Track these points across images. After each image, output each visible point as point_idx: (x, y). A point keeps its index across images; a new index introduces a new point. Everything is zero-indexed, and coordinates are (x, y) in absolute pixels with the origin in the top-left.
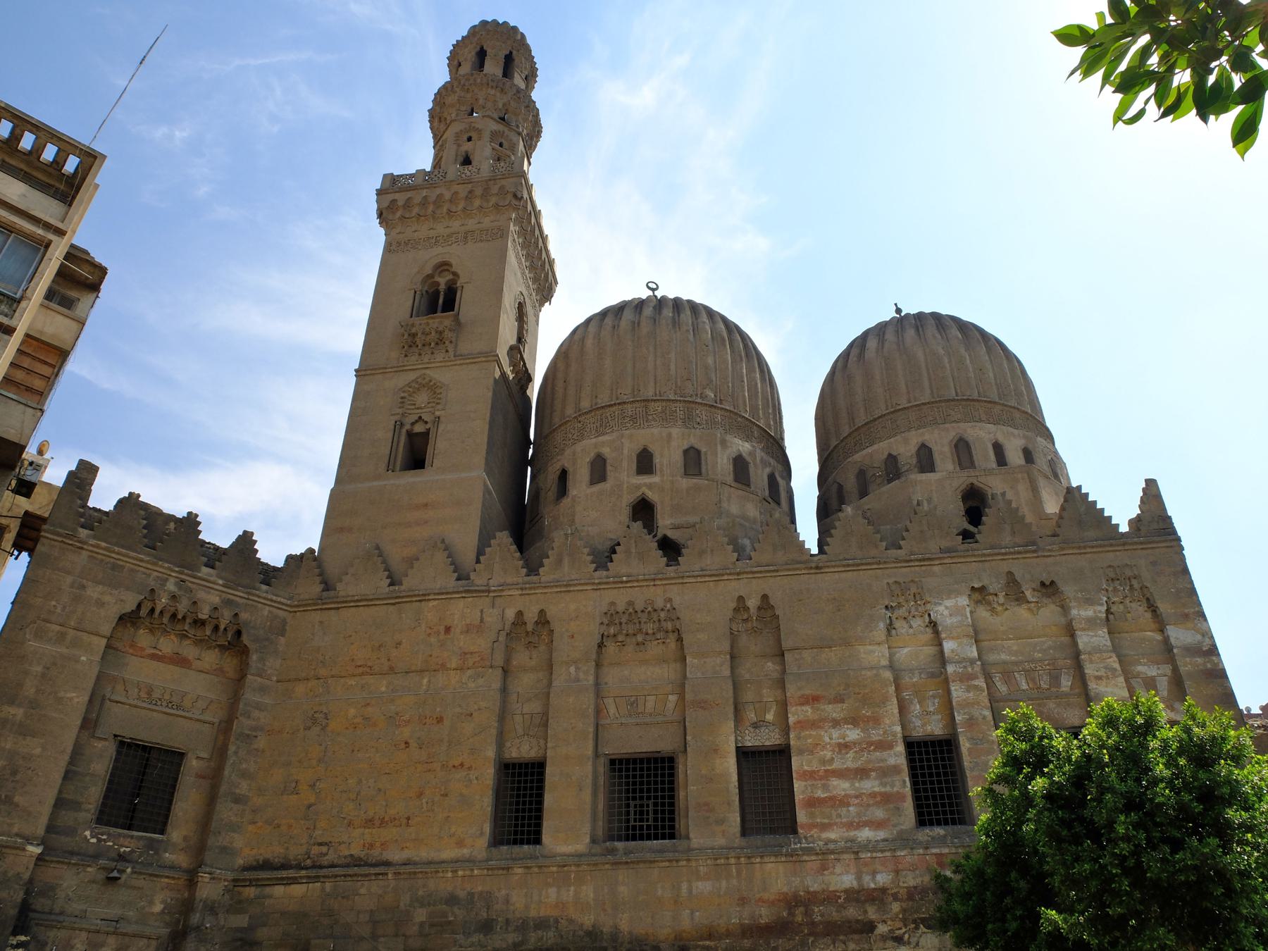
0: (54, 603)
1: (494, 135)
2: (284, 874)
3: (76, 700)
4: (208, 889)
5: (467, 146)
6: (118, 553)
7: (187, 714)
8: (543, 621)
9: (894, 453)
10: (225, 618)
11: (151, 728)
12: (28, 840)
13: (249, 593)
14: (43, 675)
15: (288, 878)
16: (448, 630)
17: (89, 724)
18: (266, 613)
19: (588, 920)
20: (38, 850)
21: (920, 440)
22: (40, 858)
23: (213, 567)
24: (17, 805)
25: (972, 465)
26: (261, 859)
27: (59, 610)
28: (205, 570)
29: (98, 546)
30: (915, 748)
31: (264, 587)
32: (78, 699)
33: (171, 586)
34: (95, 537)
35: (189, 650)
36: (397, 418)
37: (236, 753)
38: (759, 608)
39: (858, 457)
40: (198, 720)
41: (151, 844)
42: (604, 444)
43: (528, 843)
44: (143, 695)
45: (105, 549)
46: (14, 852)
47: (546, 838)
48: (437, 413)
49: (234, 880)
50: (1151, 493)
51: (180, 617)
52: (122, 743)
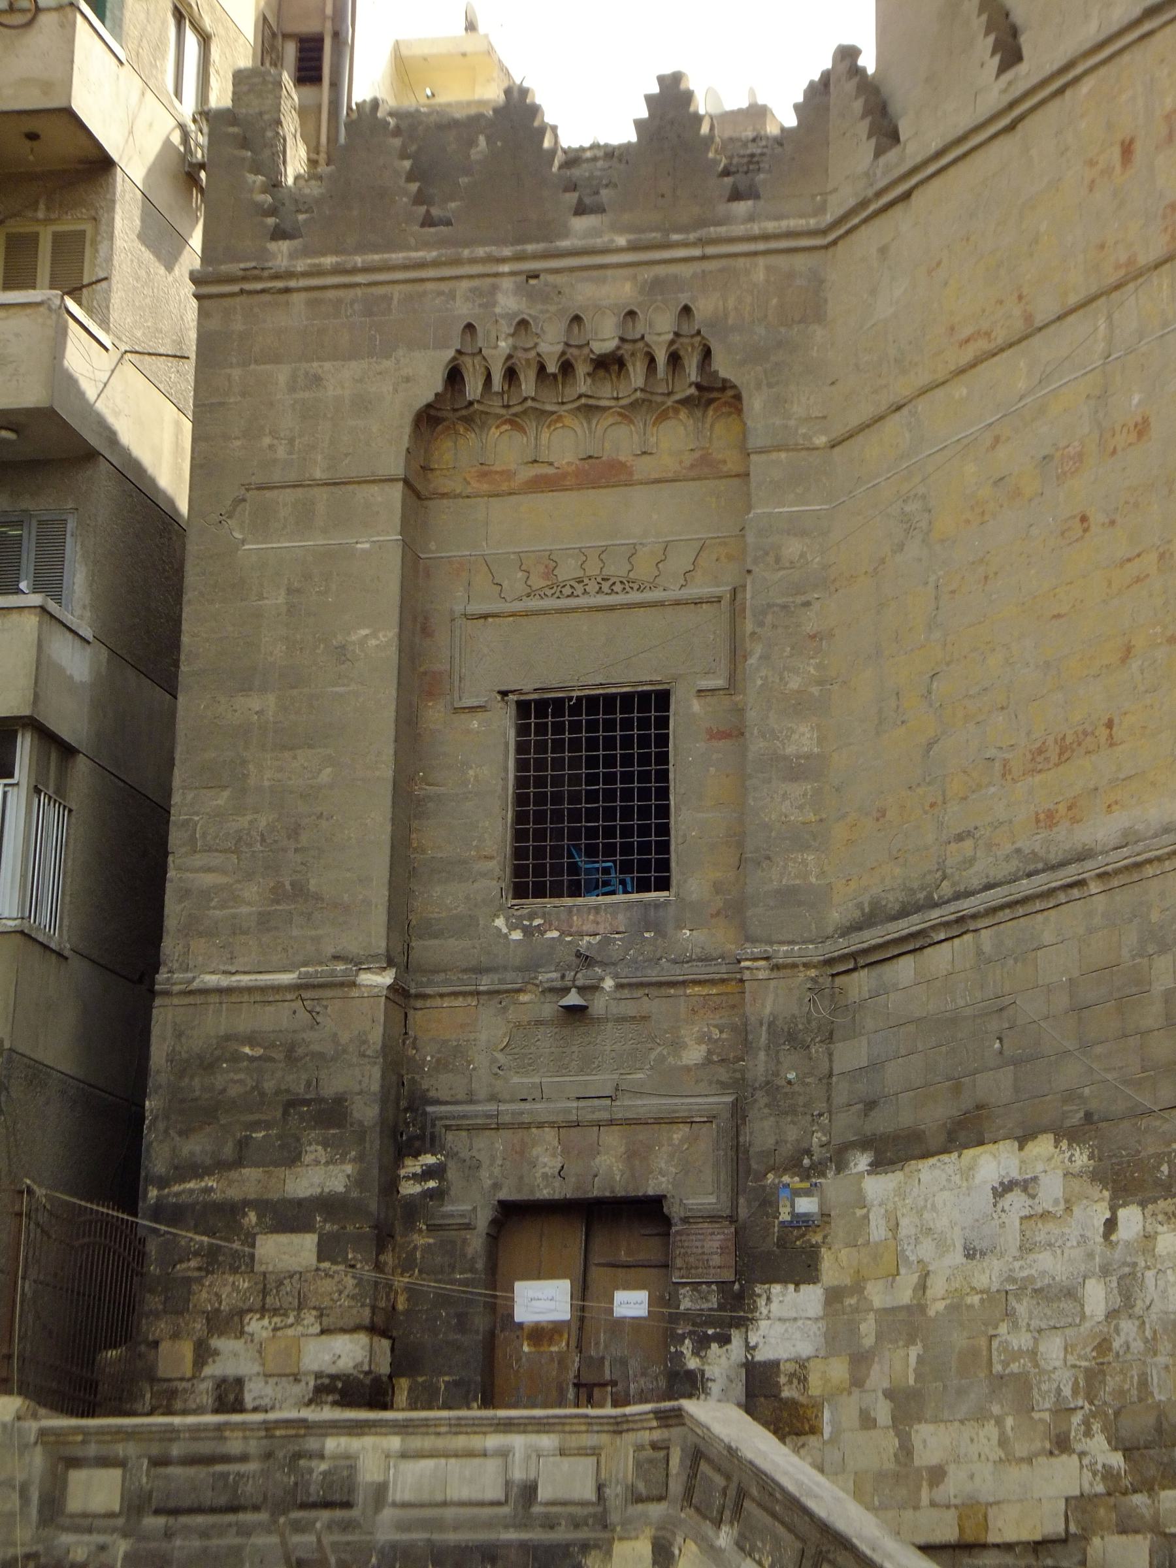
0: (267, 441)
3: (373, 642)
6: (366, 270)
7: (648, 596)
10: (660, 328)
11: (588, 659)
12: (359, 963)
13: (701, 242)
14: (291, 609)
16: (1127, 150)
17: (419, 679)
18: (759, 275)
20: (386, 979)
22: (399, 994)
23: (599, 209)
24: (318, 898)
26: (866, 899)
27: (281, 452)
28: (580, 224)
29: (319, 272)
31: (742, 207)
32: (377, 640)
33: (508, 302)
34: (306, 252)
35: (619, 440)
37: (765, 657)
40: (677, 603)
41: (650, 921)
44: (537, 582)
45: (337, 270)
46: (338, 992)
51: (552, 368)
52: (523, 708)
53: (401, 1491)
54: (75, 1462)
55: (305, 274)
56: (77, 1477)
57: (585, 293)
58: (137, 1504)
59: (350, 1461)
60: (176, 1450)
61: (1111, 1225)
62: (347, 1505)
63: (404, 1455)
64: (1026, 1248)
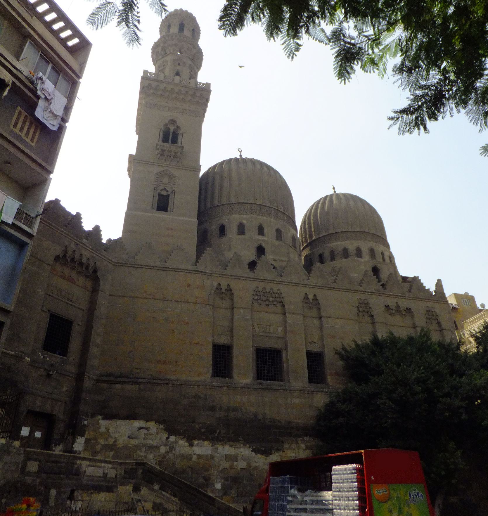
1: (190, 66)
2: (122, 379)
4: (87, 384)
5: (179, 68)
8: (229, 289)
9: (347, 248)
15: (123, 382)
19: (253, 410)
21: (357, 245)
25: (375, 259)
30: (309, 354)
33: (73, 246)
35: (74, 275)
36: (155, 186)
38: (313, 299)
39: (331, 245)
42: (244, 218)
43: (222, 377)
47: (235, 376)
48: (174, 189)
49: (97, 380)
50: (439, 284)
53: (88, 473)
54: (30, 459)
55: (44, 221)
56: (30, 463)
57: (84, 252)
58: (41, 470)
59: (80, 465)
60: (51, 459)
61: (167, 438)
62: (78, 475)
63: (89, 466)
64: (145, 439)
